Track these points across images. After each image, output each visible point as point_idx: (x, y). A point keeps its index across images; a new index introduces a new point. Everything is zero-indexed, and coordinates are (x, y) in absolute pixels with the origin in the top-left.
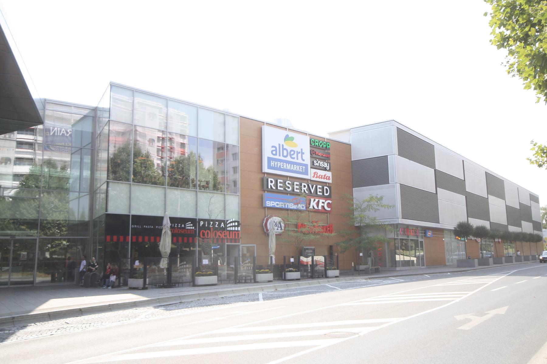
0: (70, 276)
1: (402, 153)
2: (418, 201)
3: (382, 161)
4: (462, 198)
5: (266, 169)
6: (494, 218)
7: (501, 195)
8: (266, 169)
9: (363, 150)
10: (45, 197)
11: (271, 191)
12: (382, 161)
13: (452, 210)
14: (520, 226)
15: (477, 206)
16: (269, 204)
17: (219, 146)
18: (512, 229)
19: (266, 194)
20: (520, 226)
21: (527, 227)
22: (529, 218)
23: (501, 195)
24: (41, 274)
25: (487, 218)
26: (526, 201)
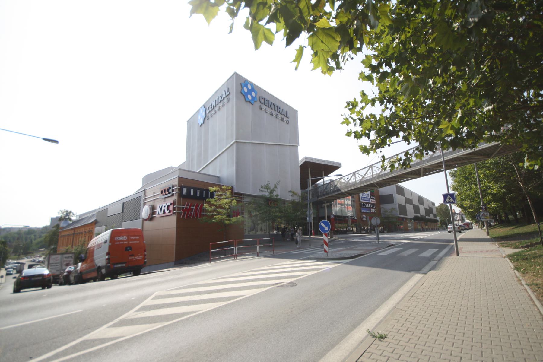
0: (352, 330)
1: (398, 193)
2: (402, 209)
3: (391, 196)
4: (412, 206)
5: (361, 200)
6: (421, 214)
7: (423, 204)
8: (361, 200)
9: (56, 224)
10: (317, 24)
11: (363, 207)
12: (391, 196)
13: (410, 213)
14: (429, 216)
15: (416, 209)
16: (363, 211)
17: (97, 225)
18: (427, 217)
19: (362, 208)
20: (429, 216)
21: (432, 217)
22: (432, 213)
23: (423, 204)
25: (419, 214)
26: (431, 206)
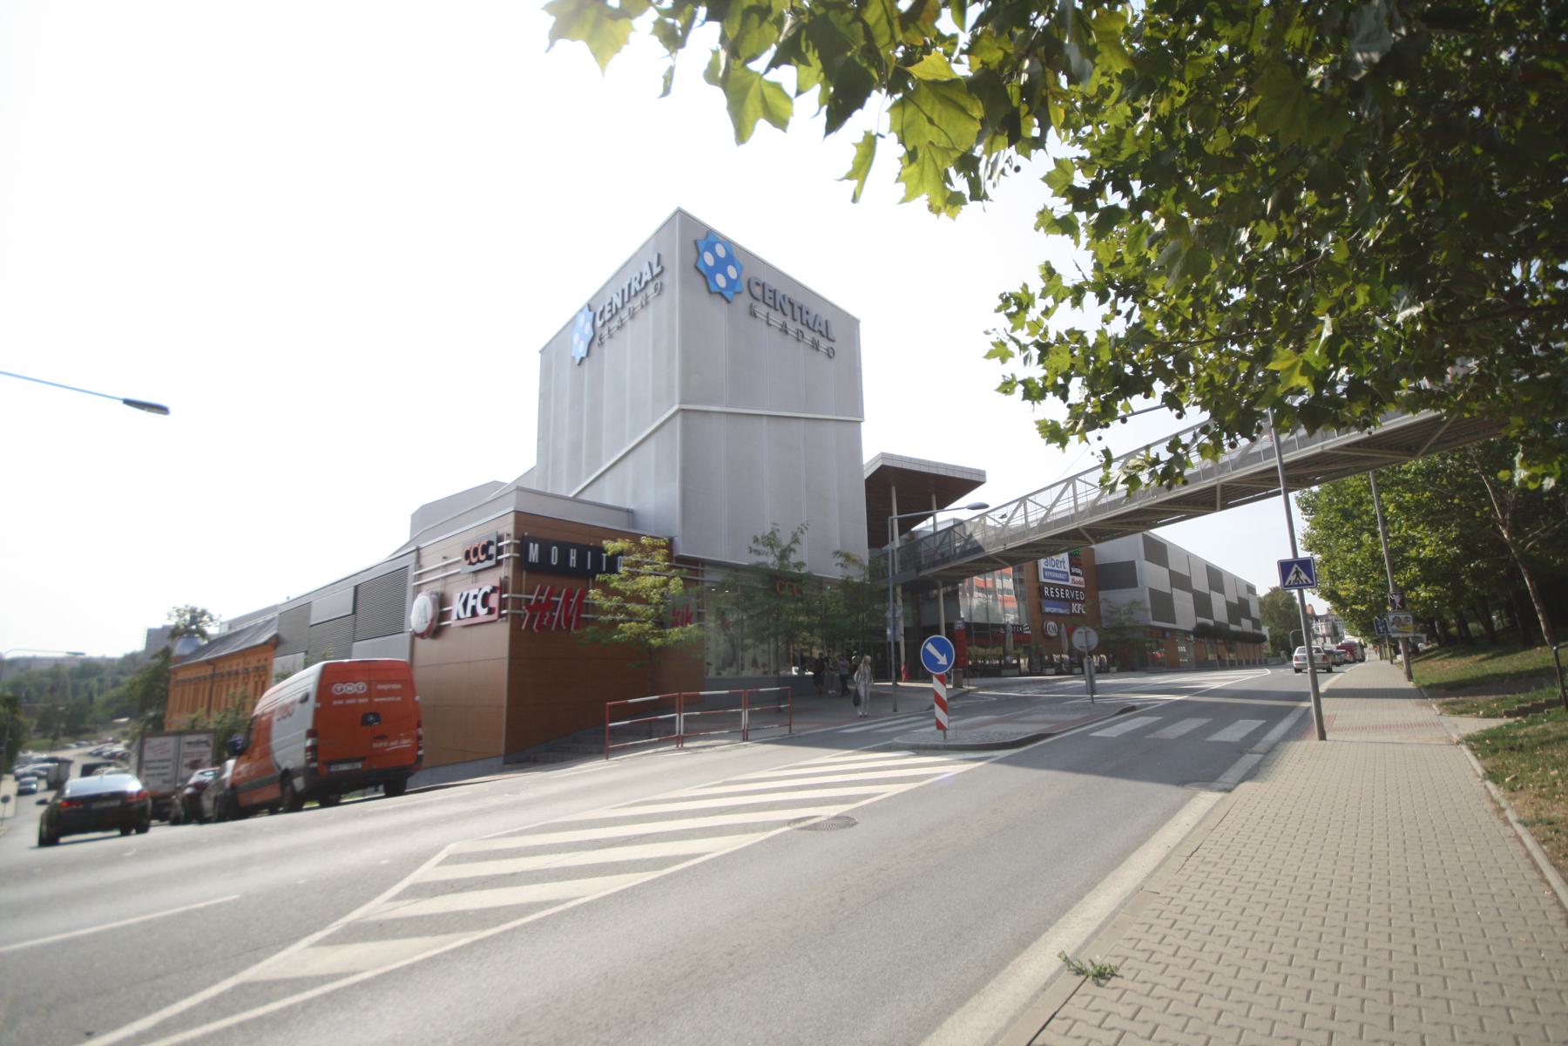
1: (1148, 558)
2: (1162, 604)
3: (1130, 566)
4: (1189, 596)
5: (1042, 579)
6: (1217, 618)
7: (1221, 590)
8: (1042, 579)
11: (1049, 598)
12: (1130, 566)
13: (1185, 615)
14: (1239, 624)
15: (1202, 604)
16: (1048, 610)
17: (280, 649)
18: (1233, 627)
19: (1044, 602)
20: (1239, 624)
21: (1246, 626)
22: (1248, 616)
23: (1221, 590)
24: (1035, 515)
25: (1211, 617)
26: (1244, 594)
